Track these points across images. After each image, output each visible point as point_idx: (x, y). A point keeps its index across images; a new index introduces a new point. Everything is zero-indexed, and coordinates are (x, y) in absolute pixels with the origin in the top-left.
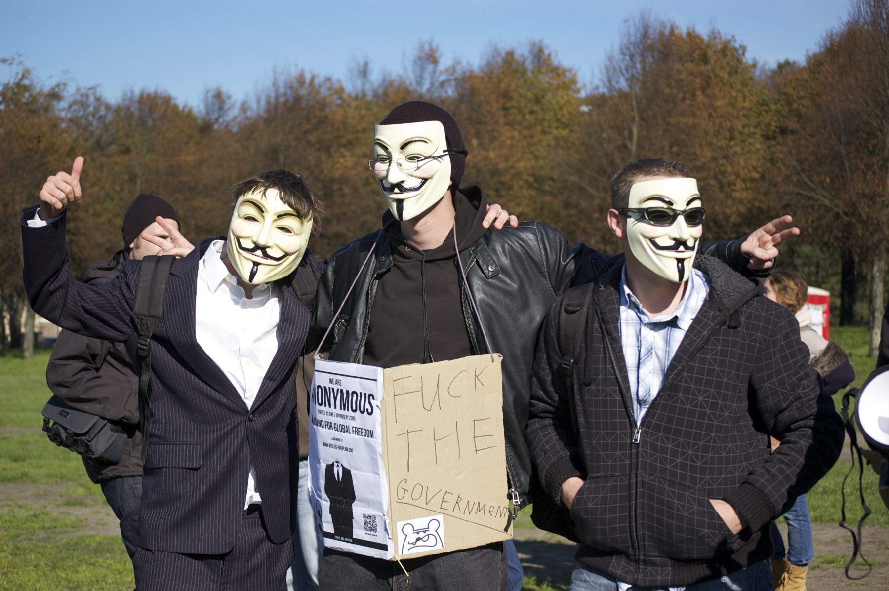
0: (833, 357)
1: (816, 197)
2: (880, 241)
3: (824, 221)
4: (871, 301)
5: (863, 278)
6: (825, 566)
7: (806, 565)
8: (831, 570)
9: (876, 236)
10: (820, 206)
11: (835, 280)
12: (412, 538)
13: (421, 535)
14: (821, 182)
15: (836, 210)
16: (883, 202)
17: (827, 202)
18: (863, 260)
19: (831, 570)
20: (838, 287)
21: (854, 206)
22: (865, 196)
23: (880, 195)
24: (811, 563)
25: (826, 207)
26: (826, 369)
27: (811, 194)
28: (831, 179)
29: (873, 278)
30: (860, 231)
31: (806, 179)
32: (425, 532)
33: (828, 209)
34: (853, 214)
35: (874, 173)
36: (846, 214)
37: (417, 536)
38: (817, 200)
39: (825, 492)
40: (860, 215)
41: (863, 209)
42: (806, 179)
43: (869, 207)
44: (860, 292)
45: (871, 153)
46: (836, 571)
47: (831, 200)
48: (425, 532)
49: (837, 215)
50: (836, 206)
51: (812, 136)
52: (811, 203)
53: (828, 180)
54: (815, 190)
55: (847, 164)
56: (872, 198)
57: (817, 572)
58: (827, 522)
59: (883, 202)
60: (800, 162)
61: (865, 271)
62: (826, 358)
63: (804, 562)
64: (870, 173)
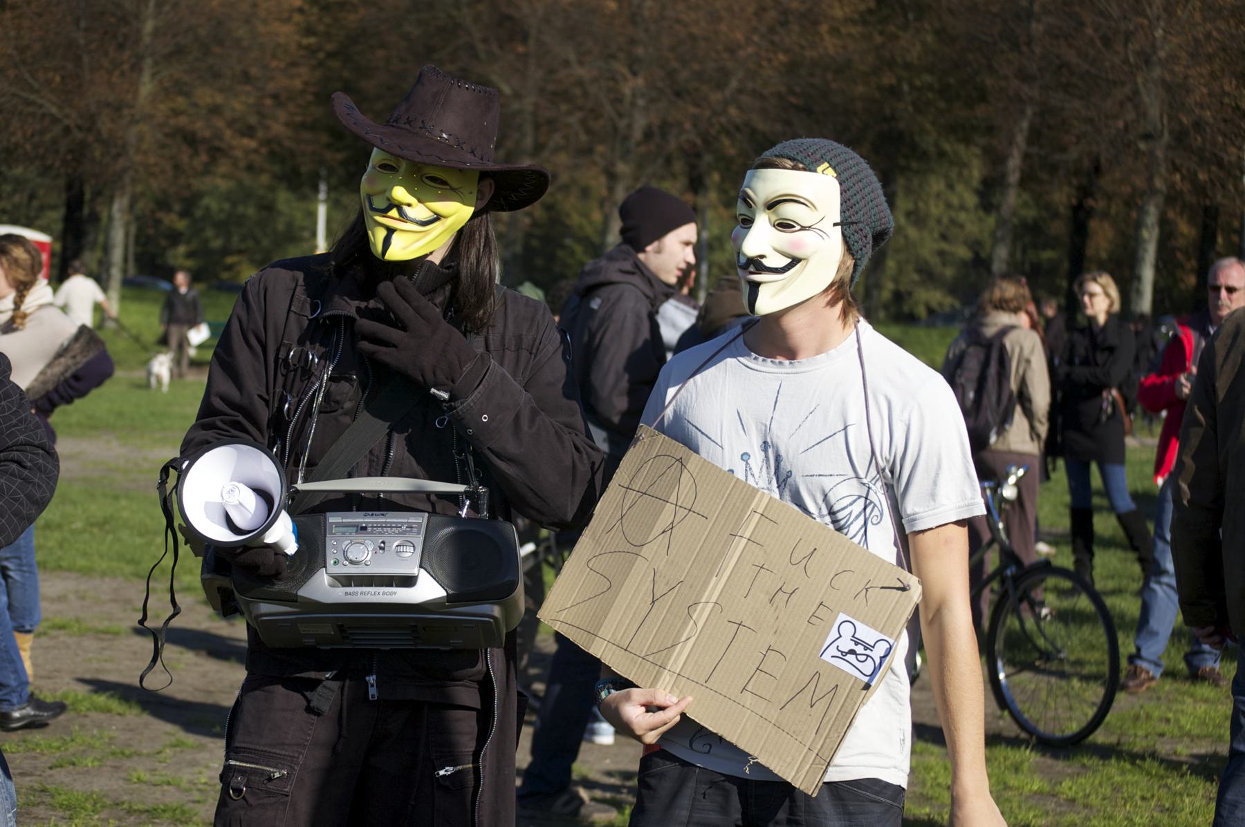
0: (88, 343)
1: (40, 101)
2: (124, 170)
3: (48, 137)
4: (107, 249)
5: (95, 218)
6: (53, 633)
7: (29, 632)
8: (62, 639)
9: (121, 163)
10: (44, 115)
11: (56, 216)
12: (847, 645)
13: (859, 649)
14: (48, 82)
15: (67, 122)
16: (133, 116)
17: (54, 110)
18: (97, 194)
19: (62, 639)
20: (59, 227)
21: (92, 118)
22: (108, 105)
23: (131, 107)
24: (40, 628)
25: (52, 116)
26: (79, 358)
27: (33, 97)
28: (63, 78)
29: (110, 218)
30: (97, 154)
31: (27, 76)
32: (866, 649)
33: (55, 120)
34: (89, 130)
35: (123, 74)
36: (79, 128)
37: (852, 646)
38: (41, 106)
39: (47, 526)
40: (99, 133)
41: (105, 125)
42: (27, 76)
43: (113, 121)
44: (91, 238)
45: (121, 47)
46: (69, 641)
47: (60, 108)
48: (866, 649)
49: (67, 130)
50: (67, 116)
51: (40, 15)
52: (31, 109)
53: (58, 79)
54: (37, 92)
55: (86, 59)
56: (118, 108)
57: (44, 641)
58: (54, 570)
59: (133, 116)
60: (22, 50)
61: (99, 208)
62: (77, 346)
63: (28, 627)
64: (117, 73)
